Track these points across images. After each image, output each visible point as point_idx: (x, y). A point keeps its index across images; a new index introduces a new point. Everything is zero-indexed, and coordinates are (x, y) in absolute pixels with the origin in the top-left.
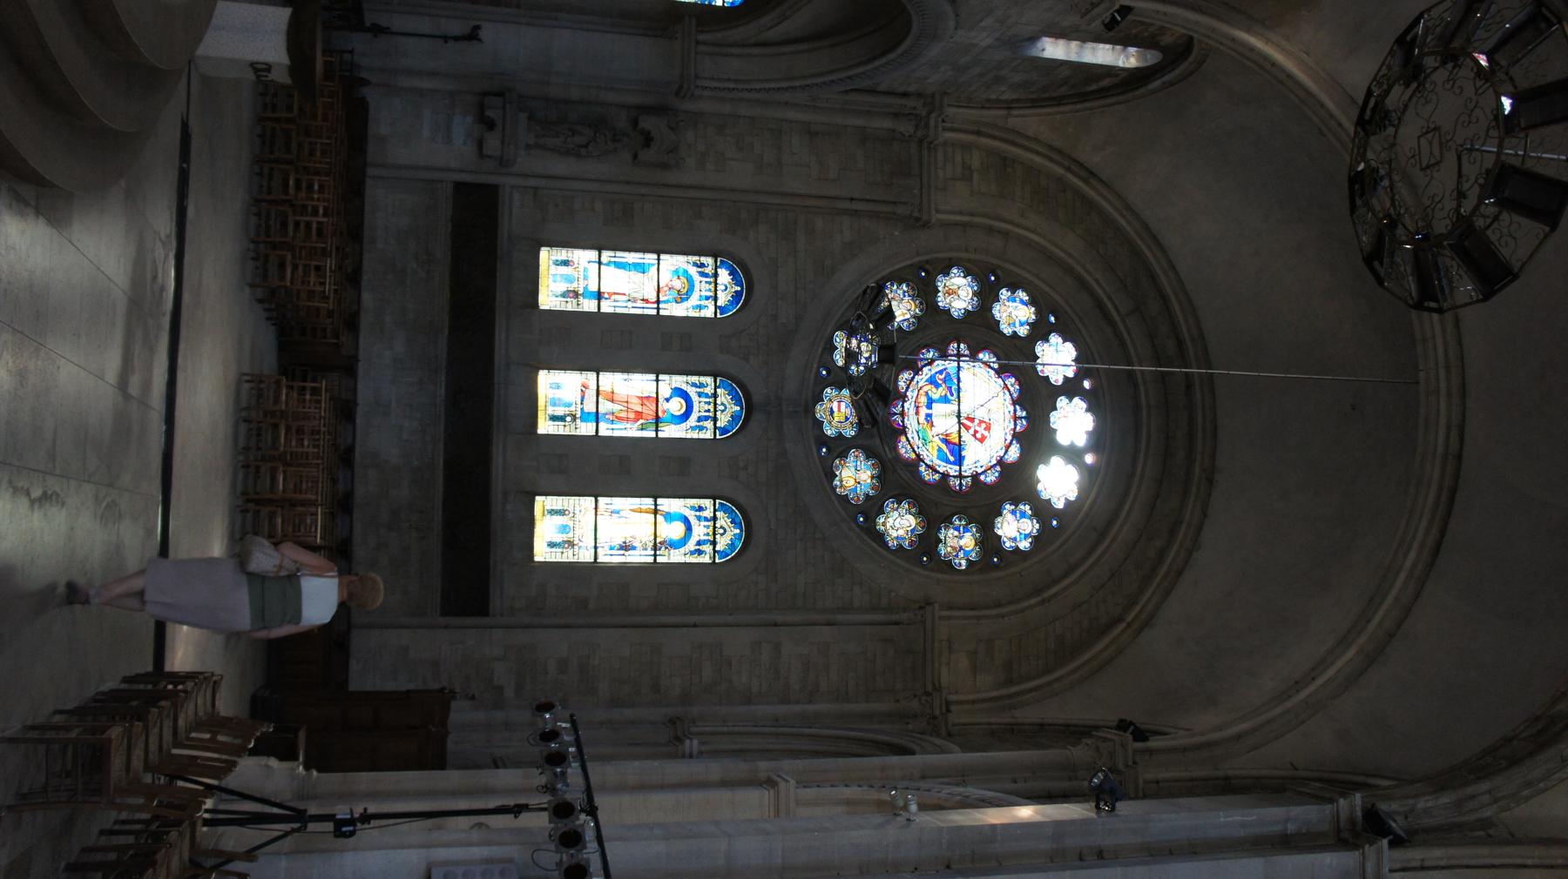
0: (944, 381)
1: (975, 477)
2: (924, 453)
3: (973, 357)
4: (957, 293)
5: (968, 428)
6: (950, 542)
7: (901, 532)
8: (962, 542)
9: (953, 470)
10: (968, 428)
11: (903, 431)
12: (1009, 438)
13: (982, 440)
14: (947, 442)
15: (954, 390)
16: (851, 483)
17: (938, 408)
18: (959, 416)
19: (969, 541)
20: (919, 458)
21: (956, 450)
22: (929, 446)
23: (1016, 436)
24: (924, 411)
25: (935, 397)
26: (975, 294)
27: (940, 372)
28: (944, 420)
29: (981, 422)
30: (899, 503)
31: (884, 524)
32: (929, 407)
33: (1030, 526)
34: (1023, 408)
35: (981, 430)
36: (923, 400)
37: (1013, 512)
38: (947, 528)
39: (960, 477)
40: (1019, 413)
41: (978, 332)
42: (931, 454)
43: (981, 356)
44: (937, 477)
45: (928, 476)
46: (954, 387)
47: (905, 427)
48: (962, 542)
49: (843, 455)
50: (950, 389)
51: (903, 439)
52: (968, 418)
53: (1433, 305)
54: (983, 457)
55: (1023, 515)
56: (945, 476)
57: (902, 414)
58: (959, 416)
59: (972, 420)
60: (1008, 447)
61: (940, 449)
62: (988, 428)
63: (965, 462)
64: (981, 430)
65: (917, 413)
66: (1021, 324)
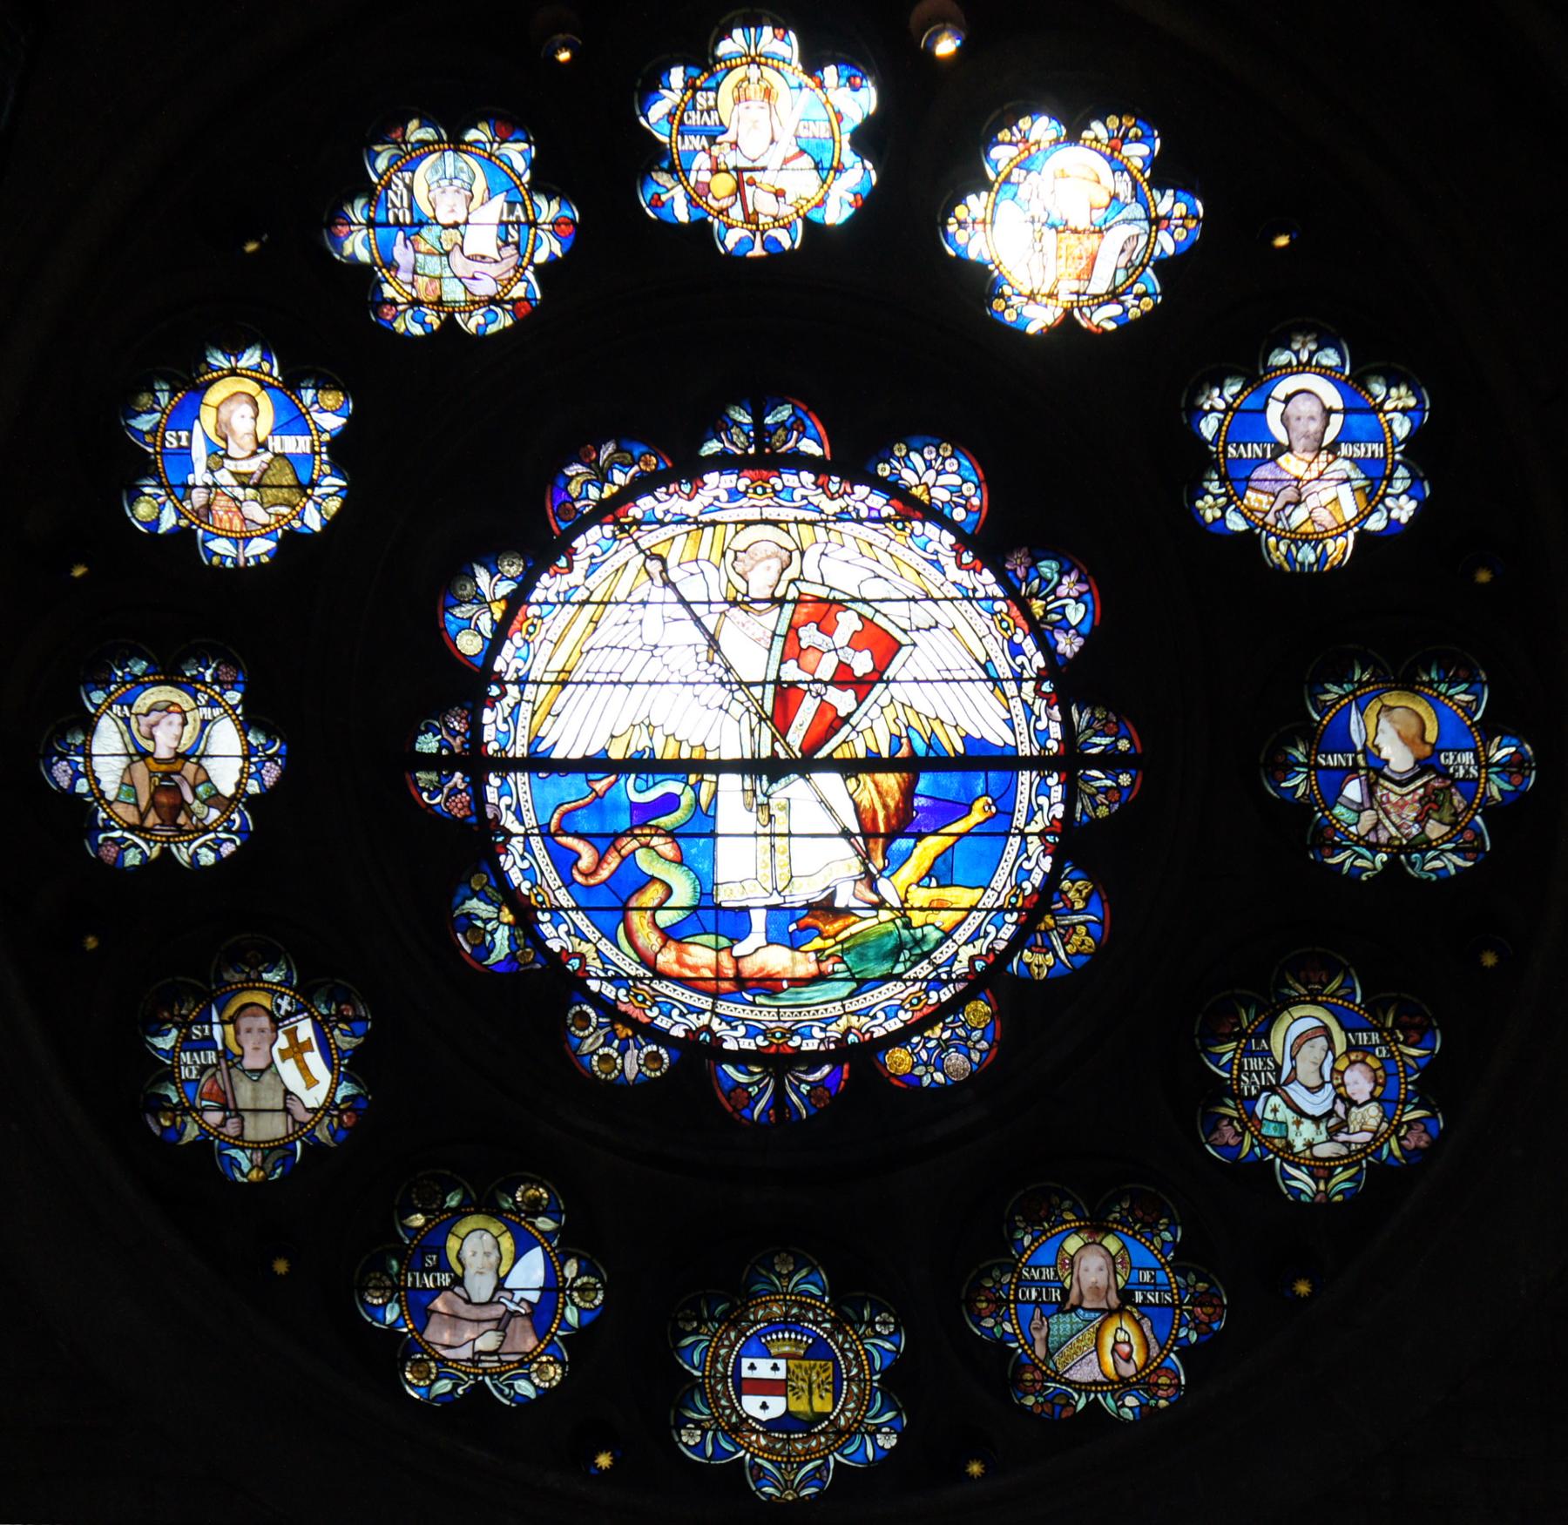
0: (605, 841)
1: (1067, 682)
2: (964, 955)
3: (473, 685)
4: (173, 753)
5: (831, 723)
6: (1401, 815)
7: (1359, 1083)
8: (1399, 758)
9: (1040, 802)
10: (831, 723)
11: (858, 1057)
12: (865, 498)
13: (885, 647)
14: (905, 823)
15: (651, 793)
16: (1122, 1331)
17: (741, 872)
18: (770, 769)
19: (1390, 731)
20: (990, 978)
21: (930, 786)
22: (928, 925)
23: (852, 461)
24: (763, 955)
25: (684, 894)
26: (170, 675)
27: (564, 862)
28: (791, 847)
29: (792, 648)
30: (1221, 1090)
31: (1321, 1169)
32: (727, 922)
33: (965, 555)
34: (718, 425)
35: (834, 647)
36: (701, 956)
37: (1237, 481)
38: (1328, 838)
39: (1068, 762)
40: (738, 443)
41: (359, 652)
42: (959, 910)
43: (472, 135)
44: (1074, 889)
45: (1075, 938)
46: (634, 790)
47: (841, 1052)
48: (1399, 758)
49: (1002, 1367)
50: (644, 814)
51: (899, 1060)
52: (780, 720)
53: (489, 938)
54: (960, 653)
55: (1246, 421)
56: (1069, 842)
57: (778, 1061)
58: (770, 769)
59: (786, 695)
60: (910, 508)
61: (940, 873)
62: (825, 610)
63: (998, 735)
64: (834, 647)
65: (769, 985)
66: (294, 421)
